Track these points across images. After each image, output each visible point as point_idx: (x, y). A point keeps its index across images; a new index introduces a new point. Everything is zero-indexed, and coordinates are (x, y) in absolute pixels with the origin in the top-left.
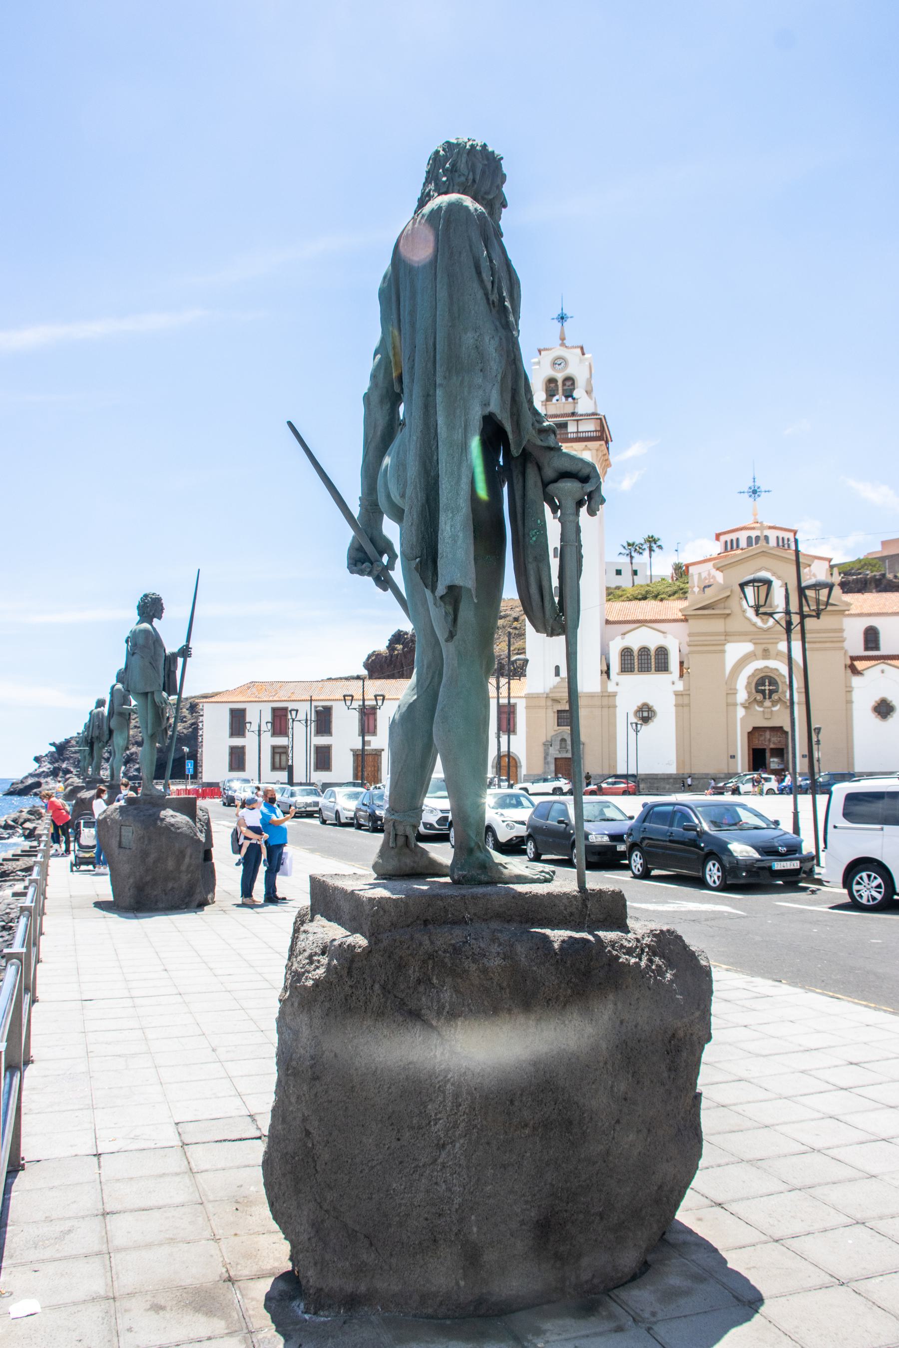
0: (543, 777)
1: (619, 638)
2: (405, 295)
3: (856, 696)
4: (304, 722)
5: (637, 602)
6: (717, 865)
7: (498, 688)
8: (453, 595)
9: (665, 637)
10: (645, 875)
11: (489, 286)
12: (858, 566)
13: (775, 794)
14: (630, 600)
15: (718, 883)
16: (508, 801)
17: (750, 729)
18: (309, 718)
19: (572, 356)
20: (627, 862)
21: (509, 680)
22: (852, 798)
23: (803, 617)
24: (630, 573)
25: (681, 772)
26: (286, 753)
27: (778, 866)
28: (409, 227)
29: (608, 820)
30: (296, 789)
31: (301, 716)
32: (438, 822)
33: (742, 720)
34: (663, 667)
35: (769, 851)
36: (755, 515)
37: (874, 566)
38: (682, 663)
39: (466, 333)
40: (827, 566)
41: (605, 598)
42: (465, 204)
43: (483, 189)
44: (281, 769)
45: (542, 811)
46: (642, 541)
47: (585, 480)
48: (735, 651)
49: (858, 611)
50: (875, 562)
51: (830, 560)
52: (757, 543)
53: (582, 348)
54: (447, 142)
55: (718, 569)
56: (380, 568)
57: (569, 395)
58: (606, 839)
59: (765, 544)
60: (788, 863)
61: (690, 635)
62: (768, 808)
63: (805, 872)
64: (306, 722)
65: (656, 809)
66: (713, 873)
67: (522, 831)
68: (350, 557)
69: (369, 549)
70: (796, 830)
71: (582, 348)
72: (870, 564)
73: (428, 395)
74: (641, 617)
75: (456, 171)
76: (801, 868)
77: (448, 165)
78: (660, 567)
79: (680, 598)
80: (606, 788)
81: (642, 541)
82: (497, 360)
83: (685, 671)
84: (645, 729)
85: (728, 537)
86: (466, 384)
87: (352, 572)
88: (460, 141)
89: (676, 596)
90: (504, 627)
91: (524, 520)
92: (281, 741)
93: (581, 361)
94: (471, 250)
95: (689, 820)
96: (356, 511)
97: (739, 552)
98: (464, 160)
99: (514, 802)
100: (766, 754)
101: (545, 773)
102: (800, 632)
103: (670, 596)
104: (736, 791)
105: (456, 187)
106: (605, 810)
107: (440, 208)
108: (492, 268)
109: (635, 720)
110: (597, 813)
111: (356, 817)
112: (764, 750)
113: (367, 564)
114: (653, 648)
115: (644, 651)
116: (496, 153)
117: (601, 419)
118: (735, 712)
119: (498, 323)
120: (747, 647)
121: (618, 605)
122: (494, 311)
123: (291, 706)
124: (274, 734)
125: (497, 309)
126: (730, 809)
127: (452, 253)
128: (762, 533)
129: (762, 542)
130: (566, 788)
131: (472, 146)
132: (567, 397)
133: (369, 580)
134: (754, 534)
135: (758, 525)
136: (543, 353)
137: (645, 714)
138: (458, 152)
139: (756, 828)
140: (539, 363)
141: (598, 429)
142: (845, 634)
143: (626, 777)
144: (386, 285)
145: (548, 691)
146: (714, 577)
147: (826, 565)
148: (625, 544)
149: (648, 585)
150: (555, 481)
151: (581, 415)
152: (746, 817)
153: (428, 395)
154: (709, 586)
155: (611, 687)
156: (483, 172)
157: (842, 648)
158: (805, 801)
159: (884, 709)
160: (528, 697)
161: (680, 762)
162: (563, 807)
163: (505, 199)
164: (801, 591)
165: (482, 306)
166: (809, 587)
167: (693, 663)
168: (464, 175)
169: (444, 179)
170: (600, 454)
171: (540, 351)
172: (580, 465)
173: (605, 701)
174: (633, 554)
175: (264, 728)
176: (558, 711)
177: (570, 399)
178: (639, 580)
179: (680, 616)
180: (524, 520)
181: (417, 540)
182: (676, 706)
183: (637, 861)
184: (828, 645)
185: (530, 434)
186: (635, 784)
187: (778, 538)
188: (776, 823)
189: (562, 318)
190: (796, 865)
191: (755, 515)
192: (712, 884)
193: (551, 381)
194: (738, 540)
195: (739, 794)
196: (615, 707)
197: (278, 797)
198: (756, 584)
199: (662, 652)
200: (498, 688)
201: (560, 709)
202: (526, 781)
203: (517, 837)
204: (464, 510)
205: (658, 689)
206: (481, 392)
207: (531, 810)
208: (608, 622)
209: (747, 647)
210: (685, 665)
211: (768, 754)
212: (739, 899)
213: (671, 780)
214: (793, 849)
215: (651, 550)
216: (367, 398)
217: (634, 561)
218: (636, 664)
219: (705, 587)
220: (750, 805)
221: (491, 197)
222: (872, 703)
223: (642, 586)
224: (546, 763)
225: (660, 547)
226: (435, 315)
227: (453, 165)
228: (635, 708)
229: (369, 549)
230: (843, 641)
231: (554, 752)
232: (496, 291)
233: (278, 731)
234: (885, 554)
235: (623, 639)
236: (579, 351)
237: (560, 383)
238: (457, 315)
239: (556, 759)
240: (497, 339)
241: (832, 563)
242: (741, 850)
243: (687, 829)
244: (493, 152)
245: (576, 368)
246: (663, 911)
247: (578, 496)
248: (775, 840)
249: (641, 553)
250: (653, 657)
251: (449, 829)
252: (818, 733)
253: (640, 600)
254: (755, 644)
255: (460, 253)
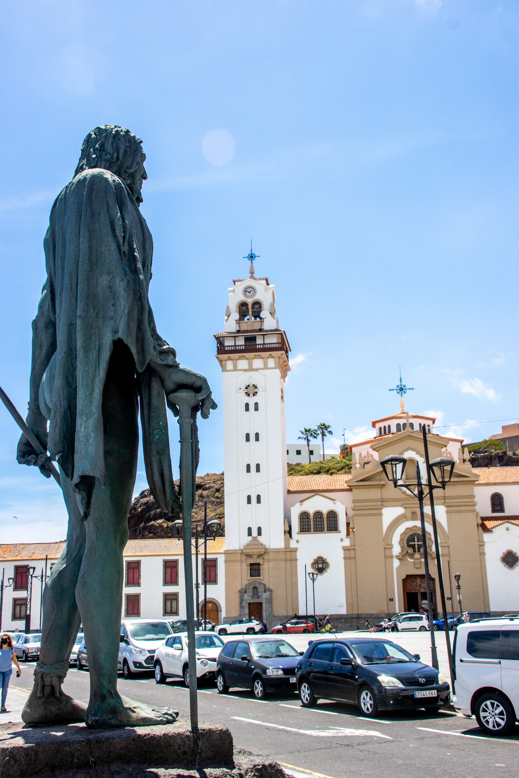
0: (239, 619)
1: (298, 505)
2: (59, 245)
3: (487, 549)
4: (39, 578)
5: (312, 475)
6: (369, 694)
7: (197, 547)
8: (86, 484)
9: (335, 504)
10: (312, 704)
11: (121, 241)
12: (484, 446)
13: (427, 630)
14: (308, 474)
15: (370, 710)
16: (203, 641)
17: (404, 577)
18: (44, 575)
19: (259, 286)
20: (297, 692)
21: (206, 540)
22: (473, 636)
23: (431, 488)
24: (308, 453)
25: (351, 613)
26: (26, 605)
27: (419, 694)
28: (63, 193)
29: (283, 656)
30: (30, 636)
31: (38, 572)
32: (146, 661)
33: (397, 570)
34: (333, 527)
35: (410, 681)
36: (402, 407)
37: (497, 446)
38: (348, 524)
39: (102, 276)
40: (460, 446)
41: (287, 474)
42: (105, 176)
43: (125, 165)
44: (20, 618)
45: (229, 649)
46: (316, 428)
47: (198, 390)
48: (390, 514)
49: (486, 481)
50: (497, 442)
51: (462, 442)
52: (404, 429)
53: (267, 280)
54: (98, 128)
55: (374, 450)
56: (44, 459)
57: (257, 315)
58: (281, 672)
59: (410, 429)
60: (428, 692)
61: (354, 501)
62: (413, 642)
63: (442, 700)
64: (42, 578)
65: (320, 646)
66: (366, 701)
67: (213, 667)
68: (19, 451)
69: (35, 444)
70: (435, 664)
71: (267, 280)
72: (494, 445)
73: (72, 324)
74: (316, 488)
75: (104, 150)
76: (438, 696)
77: (97, 146)
78: (331, 448)
79: (346, 473)
80: (290, 628)
81: (316, 428)
82: (125, 297)
83: (351, 530)
84: (320, 578)
85: (382, 425)
86: (101, 315)
87: (20, 463)
88: (108, 127)
89: (344, 470)
90: (208, 496)
91: (149, 424)
92: (22, 594)
93: (266, 290)
94: (108, 212)
95: (346, 656)
96: (24, 413)
97: (390, 436)
98: (110, 142)
99: (208, 642)
100: (420, 597)
101: (240, 615)
102: (429, 499)
103: (338, 471)
104: (394, 629)
105: (103, 163)
106: (281, 648)
107: (85, 179)
108: (124, 226)
109: (312, 571)
110: (274, 650)
111: (78, 659)
112: (417, 593)
113: (33, 456)
114: (325, 511)
115: (318, 514)
116: (137, 137)
117: (281, 334)
118: (392, 563)
119: (127, 269)
120: (399, 511)
121: (297, 479)
122: (125, 259)
123: (31, 564)
124: (16, 588)
125: (127, 258)
126: (379, 645)
127: (93, 214)
128: (408, 421)
129: (408, 429)
130: (257, 628)
131: (117, 132)
132: (255, 317)
133: (36, 469)
134: (402, 422)
135: (405, 415)
136: (236, 283)
137: (320, 566)
138: (106, 136)
139: (401, 661)
140: (234, 291)
141: (280, 341)
142: (476, 500)
143: (306, 617)
144: (48, 236)
145: (242, 547)
146: (372, 456)
147: (459, 445)
148: (303, 430)
149: (321, 462)
150: (175, 391)
151: (267, 331)
152: (392, 652)
153: (72, 324)
154: (368, 463)
155: (293, 544)
156: (125, 152)
157: (474, 511)
158: (440, 636)
159: (510, 559)
160: (227, 553)
161: (349, 605)
162: (246, 646)
163: (145, 172)
164: (430, 467)
165: (115, 255)
166: (435, 464)
167: (357, 523)
168: (110, 154)
169: (94, 156)
170: (282, 361)
171: (234, 282)
172: (193, 379)
173: (288, 556)
174: (309, 438)
175: (6, 583)
176: (251, 564)
177: (258, 319)
178: (314, 458)
179: (345, 486)
180: (149, 424)
181: (60, 439)
182: (344, 558)
183: (305, 692)
184: (463, 508)
185: (152, 355)
186: (315, 623)
187: (420, 424)
188: (417, 657)
189: (252, 257)
190: (434, 693)
191: (402, 407)
192: (366, 711)
193: (243, 305)
194: (389, 426)
195: (398, 630)
196: (296, 560)
197: (14, 643)
198: (393, 462)
199: (333, 515)
200: (197, 547)
201: (252, 562)
202: (225, 623)
203: (210, 672)
204: (96, 415)
205: (330, 546)
206: (112, 322)
207: (220, 649)
208: (289, 492)
209: (399, 511)
210: (351, 526)
211: (419, 597)
212: (388, 725)
213: (343, 620)
214: (431, 680)
215: (323, 435)
216: (35, 324)
217: (310, 444)
218: (312, 525)
219: (365, 464)
220: (395, 642)
221: (132, 171)
222: (501, 555)
223: (316, 463)
224: (242, 607)
225: (330, 433)
226: (78, 262)
227: (102, 145)
228: (312, 561)
229: (35, 444)
230: (475, 505)
231: (248, 598)
232: (126, 244)
233: (20, 586)
234: (505, 436)
235: (301, 505)
236: (264, 282)
237: (250, 306)
238: (95, 262)
239: (249, 604)
240: (125, 281)
241: (463, 444)
242: (387, 680)
243: (344, 663)
244: (134, 137)
245: (263, 295)
246: (323, 737)
247: (193, 403)
248: (417, 672)
249: (315, 437)
250: (325, 520)
251: (155, 667)
252: (458, 580)
253: (315, 474)
254: (405, 508)
255: (100, 214)
